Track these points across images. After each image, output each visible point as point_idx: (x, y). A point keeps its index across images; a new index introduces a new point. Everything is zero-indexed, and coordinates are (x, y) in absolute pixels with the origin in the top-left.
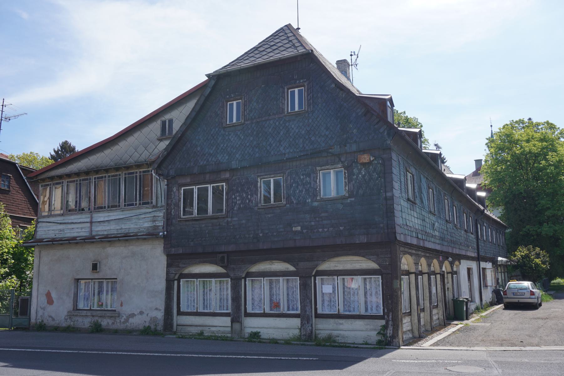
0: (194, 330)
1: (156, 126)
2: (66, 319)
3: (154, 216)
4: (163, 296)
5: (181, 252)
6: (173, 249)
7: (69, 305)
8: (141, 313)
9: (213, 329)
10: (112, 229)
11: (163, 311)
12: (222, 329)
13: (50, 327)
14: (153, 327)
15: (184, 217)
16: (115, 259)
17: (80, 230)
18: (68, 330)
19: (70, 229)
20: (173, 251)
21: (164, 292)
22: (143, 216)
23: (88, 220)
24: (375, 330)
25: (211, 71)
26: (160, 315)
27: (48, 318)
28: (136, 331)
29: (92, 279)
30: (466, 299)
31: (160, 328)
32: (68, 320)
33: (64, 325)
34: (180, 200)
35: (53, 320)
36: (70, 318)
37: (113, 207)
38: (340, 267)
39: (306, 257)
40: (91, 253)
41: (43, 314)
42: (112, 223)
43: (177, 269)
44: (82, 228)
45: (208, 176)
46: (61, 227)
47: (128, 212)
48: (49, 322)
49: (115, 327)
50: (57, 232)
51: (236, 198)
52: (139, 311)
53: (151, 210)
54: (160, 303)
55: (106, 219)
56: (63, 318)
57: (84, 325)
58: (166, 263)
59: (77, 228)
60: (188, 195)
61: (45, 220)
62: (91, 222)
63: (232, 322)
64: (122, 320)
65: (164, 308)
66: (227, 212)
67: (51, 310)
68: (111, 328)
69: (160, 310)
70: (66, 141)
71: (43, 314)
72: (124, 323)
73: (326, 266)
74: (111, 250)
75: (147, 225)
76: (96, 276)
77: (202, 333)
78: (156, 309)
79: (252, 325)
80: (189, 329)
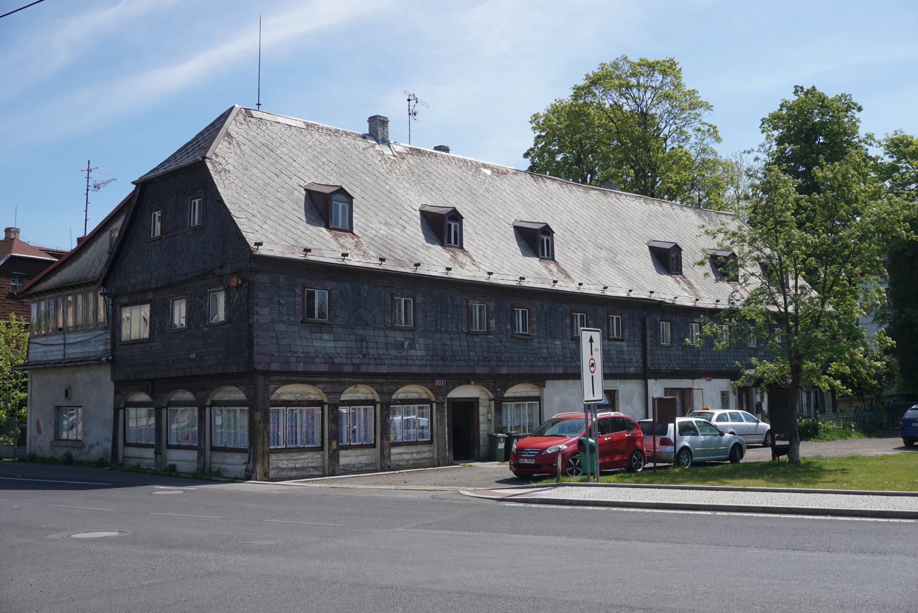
0: (134, 462)
4: (111, 426)
7: (51, 435)
8: (98, 443)
18: (52, 461)
23: (62, 342)
26: (109, 445)
33: (48, 456)
38: (227, 398)
46: (45, 349)
62: (65, 344)
63: (156, 453)
75: (101, 348)
77: (138, 466)
80: (147, 461)
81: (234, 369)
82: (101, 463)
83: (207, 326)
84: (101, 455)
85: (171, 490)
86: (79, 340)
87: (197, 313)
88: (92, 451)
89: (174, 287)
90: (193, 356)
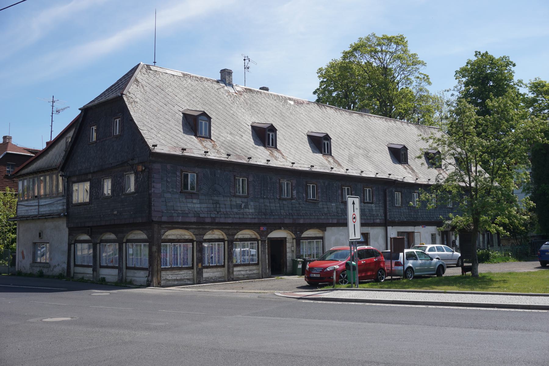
0: (80, 276)
4: (66, 254)
7: (31, 260)
8: (59, 265)
18: (31, 275)
23: (37, 204)
26: (65, 266)
33: (29, 272)
38: (136, 238)
46: (27, 208)
62: (39, 206)
63: (93, 271)
70: (321, 70)
75: (60, 208)
77: (83, 278)
80: (88, 275)
81: (140, 220)
82: (60, 277)
83: (124, 195)
84: (61, 272)
85: (102, 293)
86: (47, 203)
87: (118, 187)
88: (55, 270)
89: (104, 171)
90: (116, 212)
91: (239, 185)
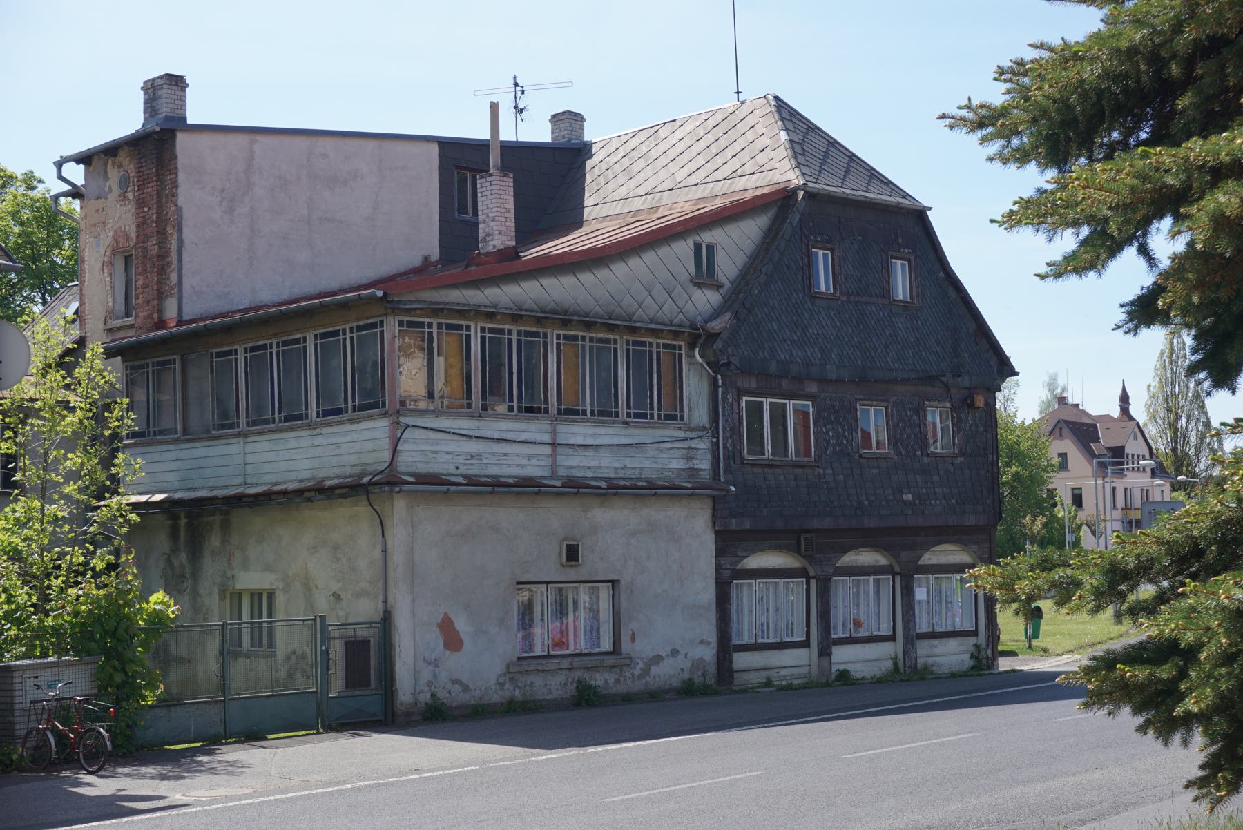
1: (683, 249)
2: (501, 685)
3: (689, 448)
5: (748, 527)
6: (734, 521)
8: (675, 653)
9: (783, 672)
10: (601, 465)
11: (714, 644)
12: (795, 671)
13: (457, 708)
14: (698, 679)
15: (751, 457)
16: (612, 532)
17: (525, 461)
19: (499, 455)
20: (734, 524)
21: (714, 607)
22: (669, 445)
23: (547, 438)
24: (965, 652)
25: (1130, 297)
26: (708, 654)
27: (449, 686)
28: (668, 691)
29: (547, 583)
30: (161, 603)
31: (711, 680)
32: (507, 686)
34: (740, 423)
35: (466, 688)
36: (512, 679)
37: (604, 413)
39: (903, 545)
40: (557, 518)
41: (435, 676)
42: (603, 450)
43: (735, 559)
44: (529, 457)
45: (784, 383)
46: (473, 447)
47: (637, 431)
48: (457, 697)
49: (622, 688)
50: (461, 459)
51: (827, 433)
52: (668, 649)
53: (682, 434)
54: (708, 629)
55: (590, 441)
56: (493, 682)
57: (550, 692)
58: (713, 547)
59: (518, 455)
60: (756, 410)
61: (420, 421)
62: (554, 445)
64: (637, 672)
65: (715, 638)
66: (819, 457)
67: (455, 664)
68: (614, 691)
69: (709, 643)
71: (435, 676)
72: (641, 677)
73: (850, 559)
74: (602, 515)
76: (571, 574)
77: (768, 683)
78: (702, 642)
79: (843, 656)
80: (783, 672)
81: (970, 520)
82: (688, 690)
83: (928, 455)
84: (686, 676)
85: (539, 755)
86: (616, 441)
87: (909, 432)
88: (654, 670)
89: (870, 383)
90: (909, 497)
91: (511, 373)
